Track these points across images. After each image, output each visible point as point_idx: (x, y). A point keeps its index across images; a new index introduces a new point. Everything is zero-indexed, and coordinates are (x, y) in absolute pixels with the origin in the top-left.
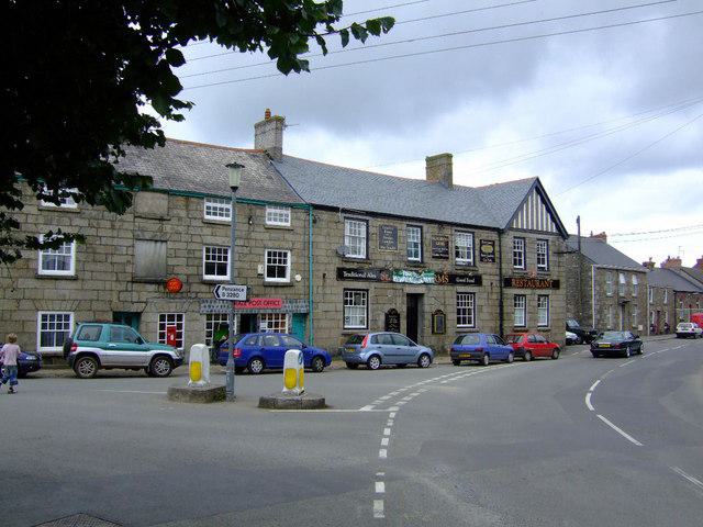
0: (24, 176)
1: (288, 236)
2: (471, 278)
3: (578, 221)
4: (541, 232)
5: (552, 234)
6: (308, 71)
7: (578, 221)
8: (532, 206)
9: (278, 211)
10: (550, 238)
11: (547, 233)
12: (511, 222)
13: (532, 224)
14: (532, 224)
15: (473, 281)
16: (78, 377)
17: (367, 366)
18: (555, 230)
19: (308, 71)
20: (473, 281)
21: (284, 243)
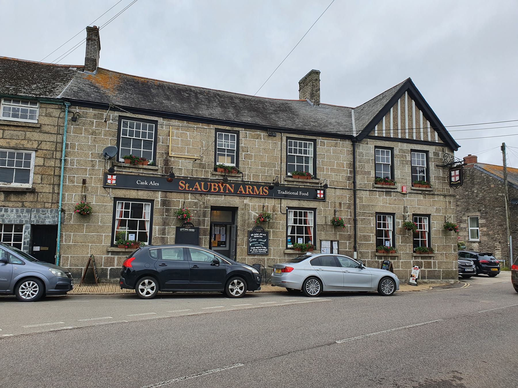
0: (479, 263)
1: (36, 135)
2: (304, 190)
3: (503, 148)
4: (418, 142)
5: (432, 143)
6: (460, 146)
7: (503, 148)
8: (403, 112)
9: (268, 182)
10: (432, 149)
11: (426, 143)
12: (370, 127)
13: (403, 129)
14: (403, 129)
15: (307, 194)
16: (137, 296)
17: (301, 292)
18: (437, 139)
19: (460, 146)
20: (307, 194)
21: (25, 142)
